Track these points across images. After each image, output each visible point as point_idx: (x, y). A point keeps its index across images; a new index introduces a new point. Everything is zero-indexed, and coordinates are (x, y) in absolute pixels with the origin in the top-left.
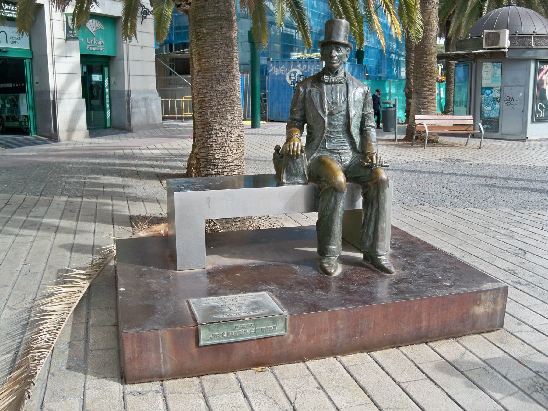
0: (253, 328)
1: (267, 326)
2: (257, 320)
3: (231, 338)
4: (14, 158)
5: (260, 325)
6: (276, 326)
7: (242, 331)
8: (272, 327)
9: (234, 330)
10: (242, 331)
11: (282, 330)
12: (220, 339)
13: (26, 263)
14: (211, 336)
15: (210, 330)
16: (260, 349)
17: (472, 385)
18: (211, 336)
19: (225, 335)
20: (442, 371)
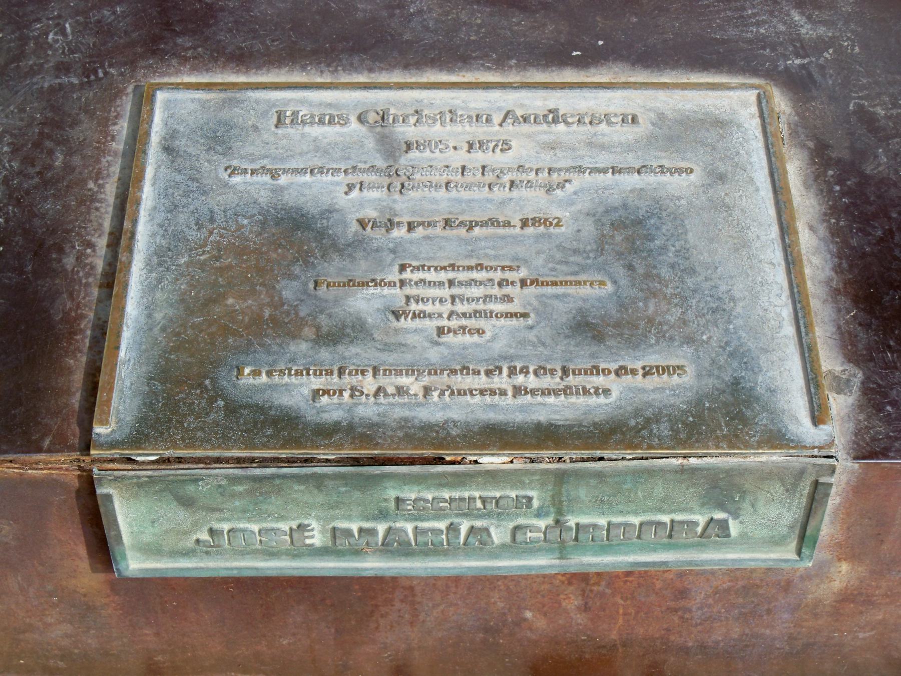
0: (539, 514)
1: (661, 511)
2: (579, 475)
3: (357, 553)
4: (327, 79)
5: (601, 506)
6: (735, 515)
7: (453, 529)
8: (701, 519)
9: (383, 515)
10: (453, 529)
11: (777, 542)
12: (271, 554)
13: (706, 534)
14: (204, 536)
15: (187, 503)
16: (585, 608)
17: (105, 366)
18: (204, 536)
19: (317, 538)
20: (456, 577)
